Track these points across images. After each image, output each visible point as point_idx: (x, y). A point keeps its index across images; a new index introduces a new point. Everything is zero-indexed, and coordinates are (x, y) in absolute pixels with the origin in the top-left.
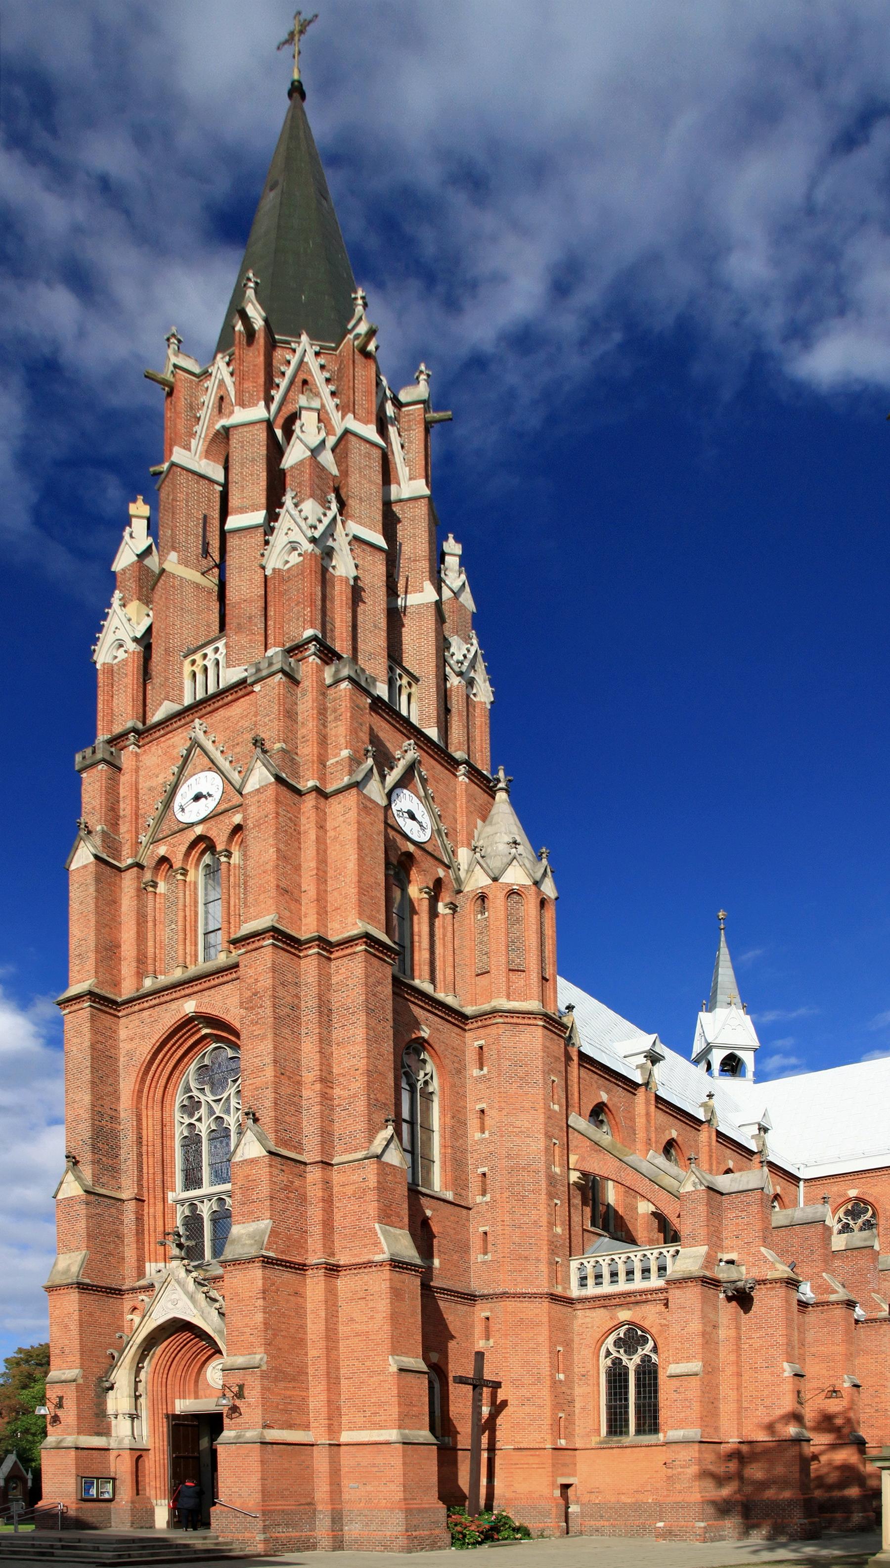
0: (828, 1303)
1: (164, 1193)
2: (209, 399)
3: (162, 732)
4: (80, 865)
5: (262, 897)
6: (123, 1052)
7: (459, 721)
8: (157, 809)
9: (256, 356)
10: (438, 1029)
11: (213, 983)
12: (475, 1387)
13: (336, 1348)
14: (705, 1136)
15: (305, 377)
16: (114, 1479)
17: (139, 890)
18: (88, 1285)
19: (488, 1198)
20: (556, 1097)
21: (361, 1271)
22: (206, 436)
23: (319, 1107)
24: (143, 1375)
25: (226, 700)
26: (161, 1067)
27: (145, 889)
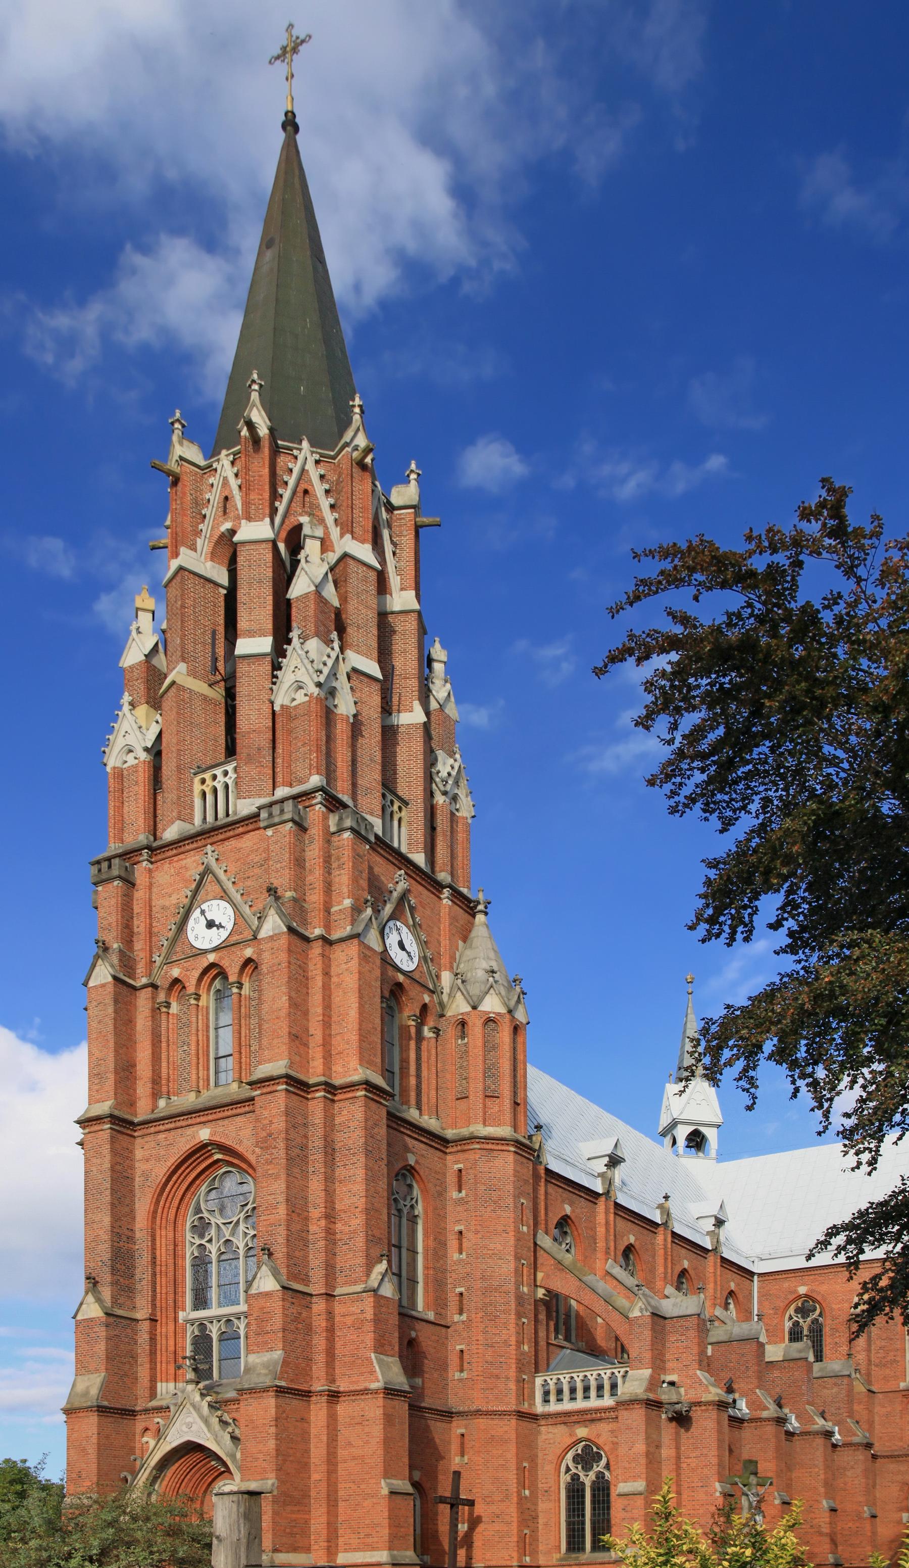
0: (760, 1420)
1: (175, 1313)
2: (214, 496)
3: (175, 852)
4: (98, 983)
5: (275, 1041)
6: (138, 1173)
10: (422, 1155)
12: (452, 1506)
14: (660, 1238)
19: (464, 1317)
20: (525, 1219)
23: (323, 1242)
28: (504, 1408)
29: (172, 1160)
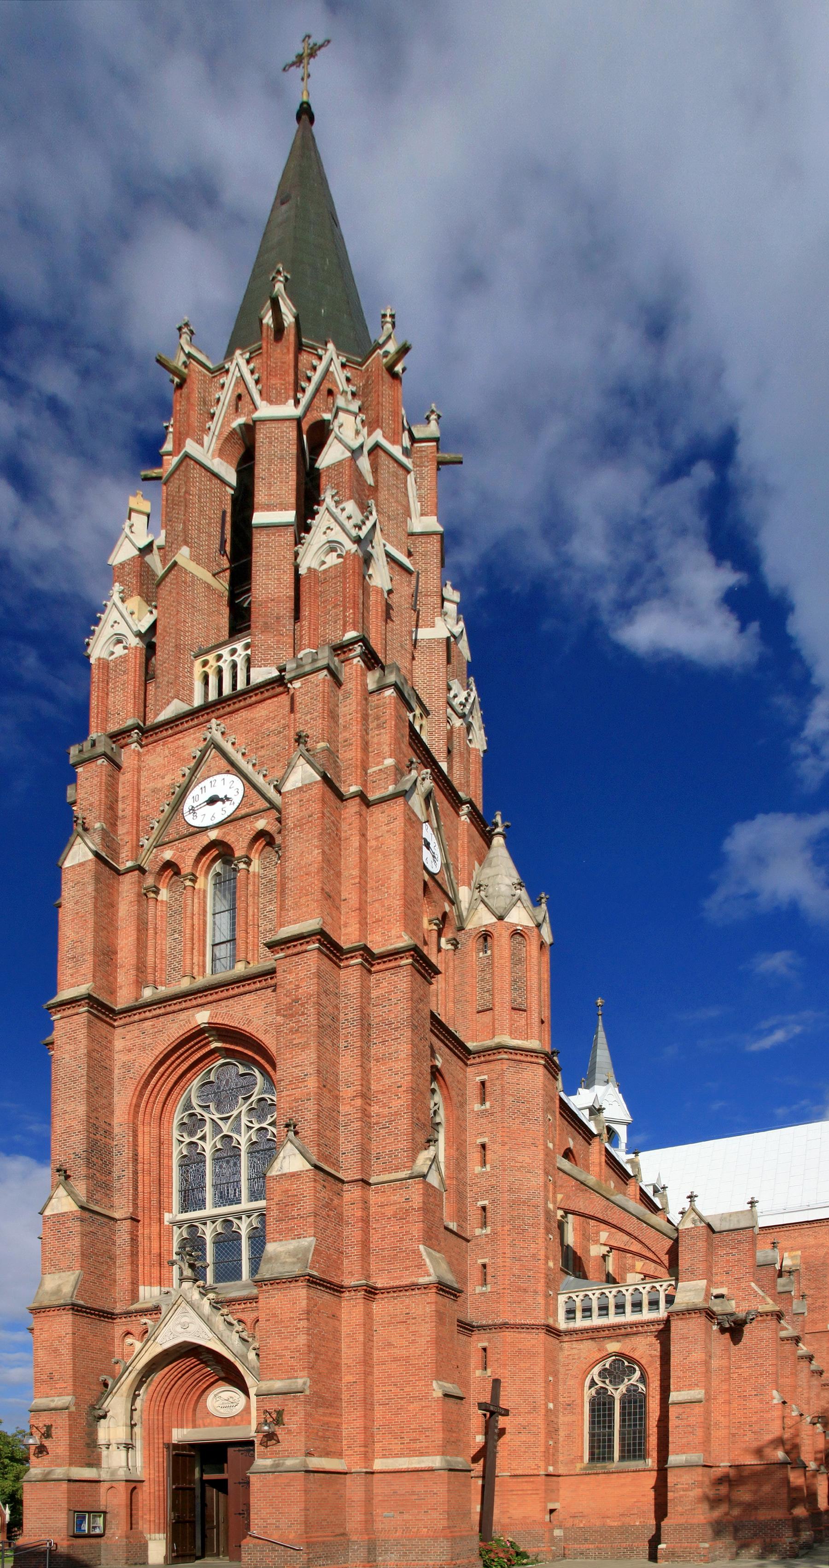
2: (227, 396)
3: (170, 732)
4: (76, 862)
5: (303, 900)
7: (461, 762)
8: (163, 811)
9: (284, 352)
11: (231, 992)
13: (371, 1373)
15: (330, 386)
16: (105, 1513)
17: (139, 895)
18: (82, 1307)
19: (488, 1230)
21: (401, 1294)
22: (220, 433)
24: (138, 1403)
25: (249, 701)
26: (161, 1081)
27: (146, 895)
28: (532, 1322)
29: (161, 1048)
